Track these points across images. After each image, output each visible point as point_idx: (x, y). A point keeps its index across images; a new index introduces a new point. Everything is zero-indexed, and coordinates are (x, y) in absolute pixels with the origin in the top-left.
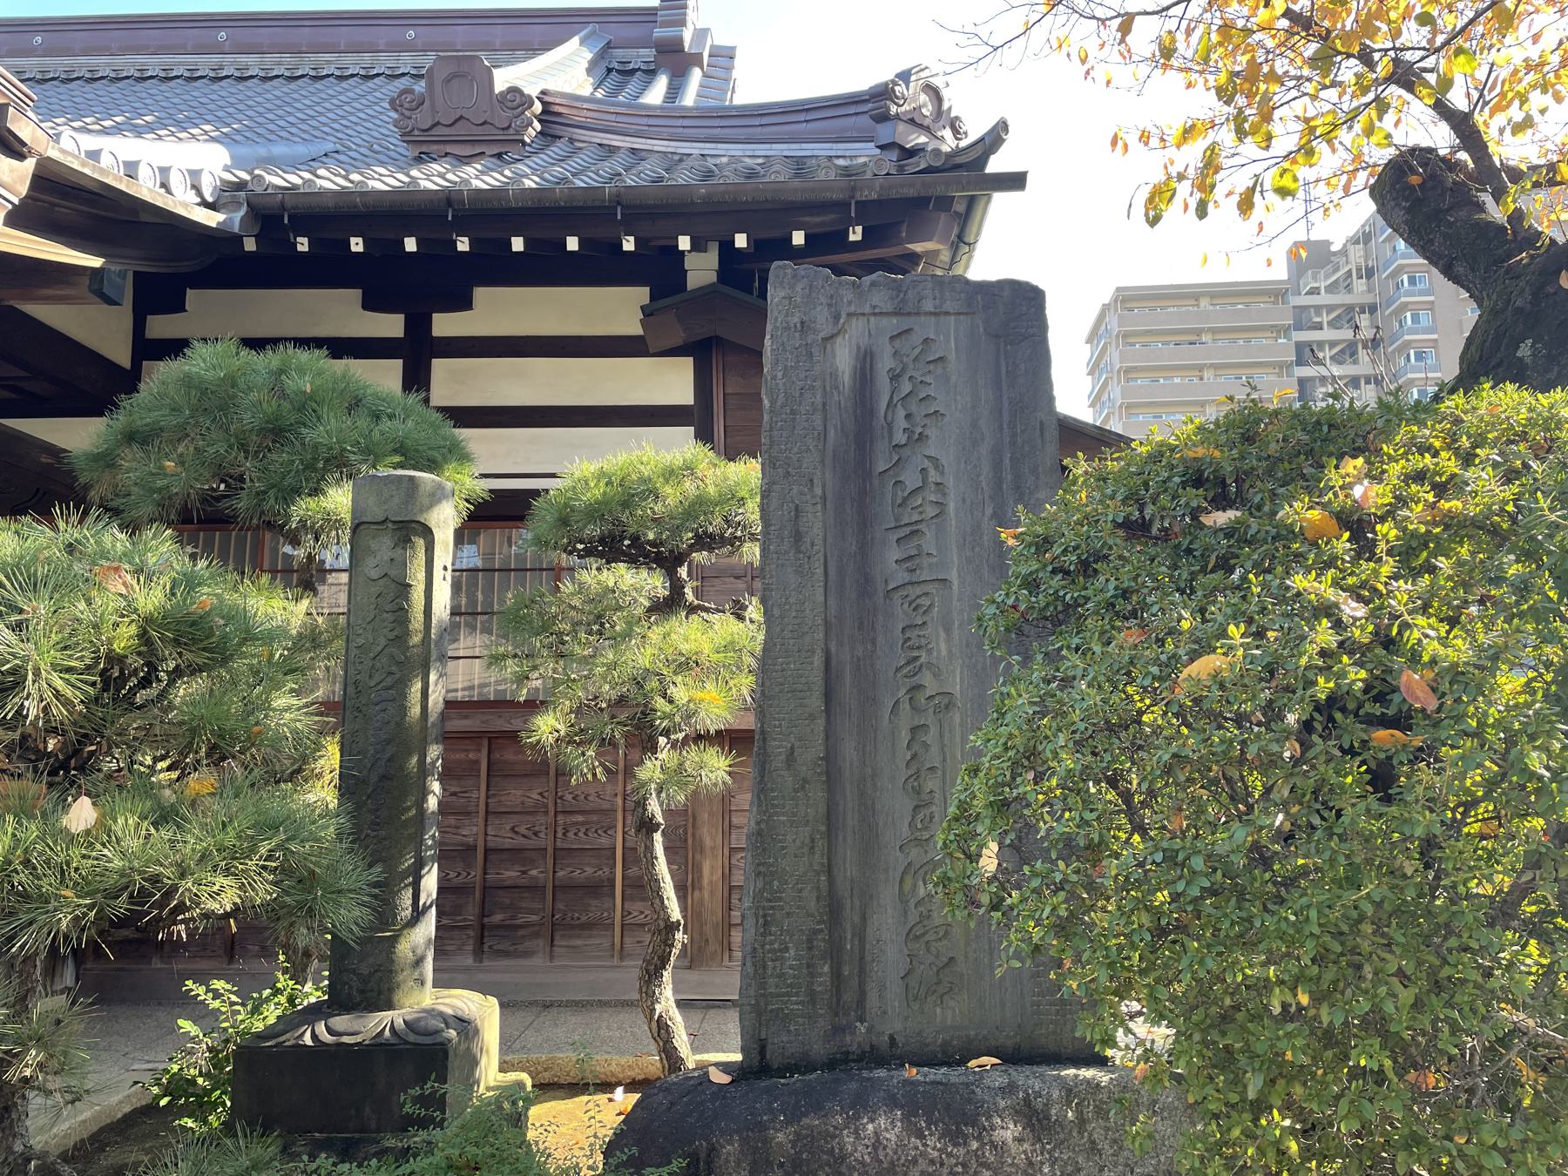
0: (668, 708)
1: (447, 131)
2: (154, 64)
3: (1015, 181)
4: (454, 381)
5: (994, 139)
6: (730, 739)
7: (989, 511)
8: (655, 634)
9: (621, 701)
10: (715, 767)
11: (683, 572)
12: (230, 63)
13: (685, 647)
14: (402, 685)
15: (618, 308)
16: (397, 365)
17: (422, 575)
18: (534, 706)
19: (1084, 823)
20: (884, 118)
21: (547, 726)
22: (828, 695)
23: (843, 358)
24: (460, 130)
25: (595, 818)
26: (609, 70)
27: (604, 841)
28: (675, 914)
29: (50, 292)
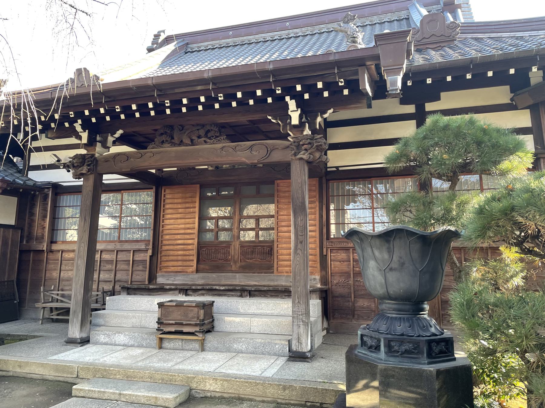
2: (268, 36)
12: (292, 33)
15: (501, 94)
24: (433, 39)
29: (352, 106)
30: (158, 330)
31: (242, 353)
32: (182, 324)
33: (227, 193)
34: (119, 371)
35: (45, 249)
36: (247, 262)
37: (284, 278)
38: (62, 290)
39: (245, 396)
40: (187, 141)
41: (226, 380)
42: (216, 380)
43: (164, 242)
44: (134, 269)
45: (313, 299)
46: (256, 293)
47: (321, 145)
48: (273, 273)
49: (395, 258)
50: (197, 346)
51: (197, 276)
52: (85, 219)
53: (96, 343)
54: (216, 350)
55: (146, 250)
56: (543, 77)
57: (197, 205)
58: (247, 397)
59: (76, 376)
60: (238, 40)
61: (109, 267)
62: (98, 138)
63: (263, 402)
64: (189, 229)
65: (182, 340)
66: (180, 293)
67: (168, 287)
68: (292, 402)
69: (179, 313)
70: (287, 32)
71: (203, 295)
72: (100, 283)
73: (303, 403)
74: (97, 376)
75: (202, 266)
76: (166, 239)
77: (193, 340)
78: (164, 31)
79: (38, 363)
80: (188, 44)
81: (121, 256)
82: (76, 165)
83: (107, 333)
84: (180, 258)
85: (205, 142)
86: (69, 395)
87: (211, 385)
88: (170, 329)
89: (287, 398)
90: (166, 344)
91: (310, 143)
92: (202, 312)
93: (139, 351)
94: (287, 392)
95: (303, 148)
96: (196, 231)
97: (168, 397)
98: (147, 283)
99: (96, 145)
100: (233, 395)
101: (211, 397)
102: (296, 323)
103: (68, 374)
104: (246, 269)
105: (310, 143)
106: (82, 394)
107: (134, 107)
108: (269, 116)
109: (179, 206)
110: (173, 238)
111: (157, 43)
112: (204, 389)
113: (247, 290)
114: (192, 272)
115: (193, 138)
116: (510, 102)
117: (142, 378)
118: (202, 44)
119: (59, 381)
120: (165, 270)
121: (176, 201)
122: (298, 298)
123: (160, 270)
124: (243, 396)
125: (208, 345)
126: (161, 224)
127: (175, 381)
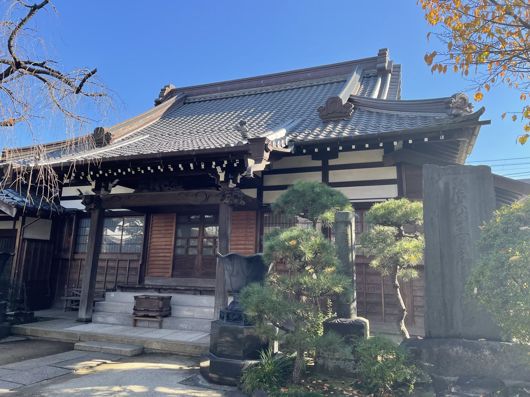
0: (403, 260)
1: (331, 115)
2: (246, 91)
3: (488, 122)
4: (334, 176)
5: (482, 111)
6: (418, 267)
7: (479, 218)
8: (398, 243)
9: (392, 258)
10: (415, 274)
11: (402, 228)
12: (264, 89)
13: (406, 247)
14: (348, 255)
15: (377, 155)
16: (320, 173)
17: (350, 232)
18: (373, 257)
19: (491, 284)
20: (449, 108)
21: (375, 263)
22: (441, 259)
23: (441, 184)
25: (376, 286)
26: (364, 77)
27: (378, 292)
28: (404, 308)
31: (185, 330)
32: (148, 310)
35: (69, 258)
40: (158, 188)
43: (151, 255)
46: (205, 292)
47: (237, 195)
49: (235, 270)
50: (157, 325)
51: (171, 279)
53: (96, 322)
54: (169, 328)
55: (138, 260)
56: (403, 145)
57: (174, 228)
60: (224, 94)
61: (112, 271)
62: (103, 185)
63: (184, 355)
64: (167, 245)
65: (149, 321)
66: (155, 291)
70: (261, 88)
75: (175, 273)
76: (152, 252)
80: (186, 96)
81: (121, 264)
84: (161, 266)
85: (169, 189)
86: (73, 349)
88: (142, 314)
90: (139, 324)
91: (230, 193)
92: (161, 303)
93: (121, 327)
94: (197, 349)
96: (172, 247)
99: (100, 190)
101: (155, 353)
105: (230, 193)
106: (80, 348)
109: (162, 229)
111: (162, 96)
114: (169, 277)
118: (197, 97)
120: (150, 275)
121: (160, 225)
126: (149, 241)
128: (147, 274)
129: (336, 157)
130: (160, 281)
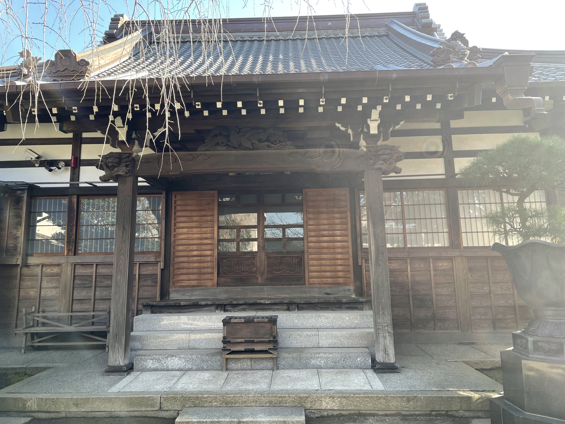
30: (224, 349)
32: (253, 342)
33: (228, 199)
34: (216, 398)
35: (19, 262)
36: (274, 274)
37: (317, 290)
38: (44, 312)
39: (366, 412)
41: (345, 397)
42: (333, 398)
44: (141, 284)
45: (366, 310)
48: (304, 284)
52: (124, 228)
54: (292, 367)
55: (156, 263)
58: (368, 412)
59: (158, 408)
63: (386, 415)
65: (251, 359)
67: (203, 303)
68: (417, 413)
69: (249, 330)
71: (244, 310)
72: (96, 301)
73: (428, 412)
74: (187, 406)
75: (222, 280)
76: (180, 249)
77: (263, 358)
78: (122, 16)
79: (104, 399)
82: (110, 165)
83: (157, 357)
85: (268, 146)
87: (327, 403)
89: (412, 409)
94: (411, 403)
95: (381, 157)
97: (298, 420)
98: (158, 299)
100: (353, 412)
102: (382, 335)
103: (147, 406)
104: (274, 280)
107: (240, 104)
108: (338, 123)
109: (194, 214)
110: (188, 249)
112: (320, 408)
113: (295, 303)
115: (253, 141)
116: (523, 124)
117: (245, 402)
119: (135, 417)
122: (382, 309)
123: (173, 284)
124: (363, 412)
125: (282, 363)
126: (173, 233)
127: (286, 403)
128: (173, 284)
129: (461, 116)
130: (198, 293)
